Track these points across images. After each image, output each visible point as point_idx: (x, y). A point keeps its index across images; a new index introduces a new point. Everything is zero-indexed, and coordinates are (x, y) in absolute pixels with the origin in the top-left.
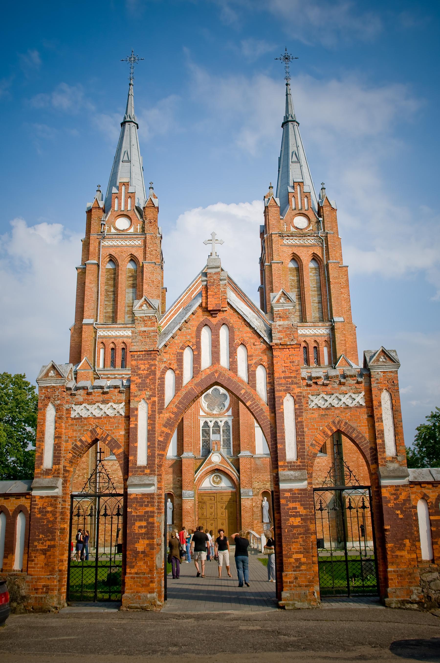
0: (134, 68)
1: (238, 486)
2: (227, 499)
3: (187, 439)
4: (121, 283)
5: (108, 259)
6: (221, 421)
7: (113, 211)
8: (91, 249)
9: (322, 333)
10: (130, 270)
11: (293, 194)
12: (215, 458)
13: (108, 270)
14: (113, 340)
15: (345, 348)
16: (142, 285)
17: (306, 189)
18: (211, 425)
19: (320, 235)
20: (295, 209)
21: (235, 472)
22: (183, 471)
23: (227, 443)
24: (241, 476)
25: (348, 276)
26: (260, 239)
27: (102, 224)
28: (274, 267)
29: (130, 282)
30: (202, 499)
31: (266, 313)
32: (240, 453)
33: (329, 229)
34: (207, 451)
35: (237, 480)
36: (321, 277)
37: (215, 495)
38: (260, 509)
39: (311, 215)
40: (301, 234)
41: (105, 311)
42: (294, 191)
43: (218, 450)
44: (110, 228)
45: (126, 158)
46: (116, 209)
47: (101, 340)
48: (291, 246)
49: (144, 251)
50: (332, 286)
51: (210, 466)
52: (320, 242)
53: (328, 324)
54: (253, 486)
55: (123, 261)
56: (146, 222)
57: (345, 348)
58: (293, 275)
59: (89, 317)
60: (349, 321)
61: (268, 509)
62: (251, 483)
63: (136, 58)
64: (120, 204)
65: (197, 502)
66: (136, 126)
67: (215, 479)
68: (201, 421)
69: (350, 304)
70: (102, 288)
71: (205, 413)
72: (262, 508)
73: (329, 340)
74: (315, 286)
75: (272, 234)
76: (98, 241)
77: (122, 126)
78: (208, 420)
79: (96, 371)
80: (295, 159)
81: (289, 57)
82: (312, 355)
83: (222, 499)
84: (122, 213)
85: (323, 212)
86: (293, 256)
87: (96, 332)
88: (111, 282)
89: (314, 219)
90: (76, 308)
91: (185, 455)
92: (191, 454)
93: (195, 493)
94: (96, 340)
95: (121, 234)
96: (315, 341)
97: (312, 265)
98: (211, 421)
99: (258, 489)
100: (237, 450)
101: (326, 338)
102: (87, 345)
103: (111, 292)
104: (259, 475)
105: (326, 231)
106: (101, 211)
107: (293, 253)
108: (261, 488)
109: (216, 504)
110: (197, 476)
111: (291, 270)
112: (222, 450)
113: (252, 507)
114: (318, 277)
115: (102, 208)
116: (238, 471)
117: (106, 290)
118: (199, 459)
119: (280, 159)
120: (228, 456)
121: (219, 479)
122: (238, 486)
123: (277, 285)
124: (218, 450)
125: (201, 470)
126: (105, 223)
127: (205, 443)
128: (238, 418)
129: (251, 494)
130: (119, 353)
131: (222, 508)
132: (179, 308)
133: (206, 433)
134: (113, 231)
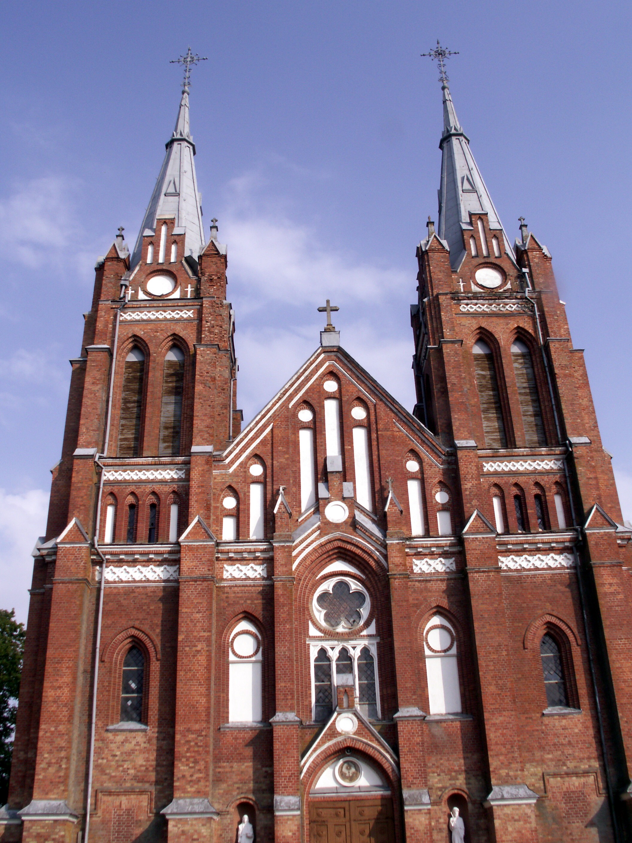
0: (191, 71)
1: (395, 784)
2: (371, 813)
3: (283, 684)
4: (153, 385)
5: (131, 345)
6: (354, 648)
7: (143, 264)
8: (100, 325)
9: (548, 468)
10: (171, 364)
11: (471, 233)
12: (345, 724)
13: (130, 365)
14: (132, 488)
15: (597, 492)
16: (194, 387)
17: (494, 224)
18: (334, 655)
19: (527, 294)
20: (477, 256)
21: (388, 752)
22: (276, 753)
23: (367, 693)
24: (402, 760)
25: (585, 368)
26: (412, 329)
27: (122, 285)
28: (447, 349)
29: (170, 385)
30: (318, 815)
31: (436, 433)
32: (397, 711)
33: (542, 286)
34: (327, 708)
35: (393, 770)
36: (536, 369)
37: (346, 805)
38: (445, 834)
39: (507, 266)
40: (491, 294)
41: (120, 437)
42: (472, 228)
43: (350, 707)
44: (137, 292)
45: (171, 190)
46: (149, 260)
47: (109, 489)
48: (475, 315)
49: (198, 329)
50: (559, 381)
51: (334, 741)
52: (528, 308)
53: (558, 450)
54: (429, 783)
55: (158, 345)
56: (204, 279)
57: (597, 492)
58: (481, 367)
59: (87, 445)
60: (595, 445)
61: (462, 833)
62: (424, 775)
63: (195, 58)
64: (156, 254)
65: (306, 822)
66: (191, 147)
67: (344, 770)
68: (311, 648)
69: (595, 417)
70: (116, 393)
71: (320, 630)
72: (450, 832)
73: (563, 480)
74: (525, 385)
75: (438, 295)
76: (112, 313)
77: (167, 148)
78: (327, 645)
79: (96, 546)
80: (467, 186)
81: (444, 51)
82: (532, 510)
83: (361, 814)
84: (160, 267)
85: (528, 260)
86: (480, 333)
87: (99, 474)
88: (135, 386)
89: (512, 272)
90: (65, 432)
91: (279, 717)
92: (292, 716)
93: (302, 801)
94: (98, 488)
95: (158, 301)
96: (537, 484)
97: (516, 349)
98: (333, 648)
99: (440, 789)
100: (391, 703)
101: (557, 478)
102: (79, 495)
103: (134, 402)
104: (441, 759)
105: (537, 289)
106: (122, 264)
107: (480, 328)
108: (445, 788)
109: (348, 825)
110: (305, 763)
111: (477, 357)
112: (358, 707)
113: (430, 830)
114: (530, 371)
115: (124, 260)
116: (395, 749)
117: (124, 399)
118: (310, 727)
119: (440, 193)
120: (372, 720)
121: (353, 770)
122: (395, 784)
123: (455, 381)
124: (350, 707)
125: (315, 750)
126: (127, 283)
127: (321, 695)
128: (389, 639)
129: (426, 799)
130: (144, 514)
131: (362, 833)
132: (265, 426)
133: (323, 672)
134: (141, 296)
